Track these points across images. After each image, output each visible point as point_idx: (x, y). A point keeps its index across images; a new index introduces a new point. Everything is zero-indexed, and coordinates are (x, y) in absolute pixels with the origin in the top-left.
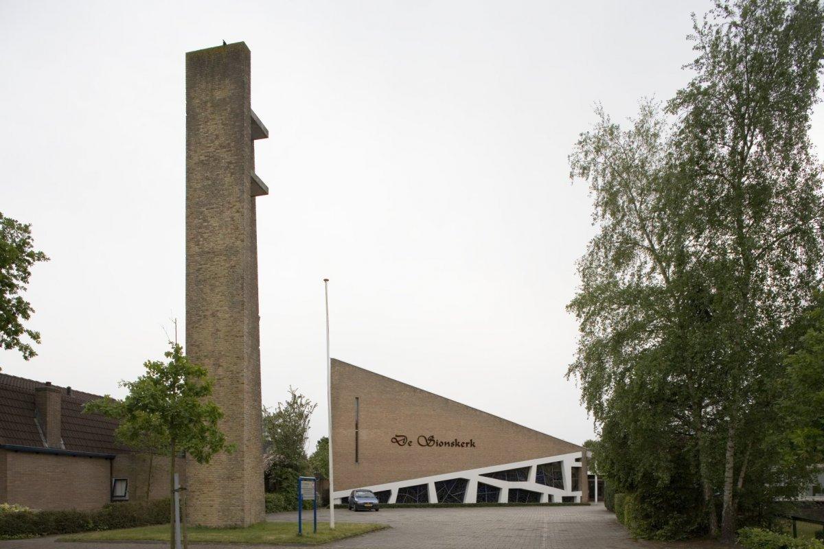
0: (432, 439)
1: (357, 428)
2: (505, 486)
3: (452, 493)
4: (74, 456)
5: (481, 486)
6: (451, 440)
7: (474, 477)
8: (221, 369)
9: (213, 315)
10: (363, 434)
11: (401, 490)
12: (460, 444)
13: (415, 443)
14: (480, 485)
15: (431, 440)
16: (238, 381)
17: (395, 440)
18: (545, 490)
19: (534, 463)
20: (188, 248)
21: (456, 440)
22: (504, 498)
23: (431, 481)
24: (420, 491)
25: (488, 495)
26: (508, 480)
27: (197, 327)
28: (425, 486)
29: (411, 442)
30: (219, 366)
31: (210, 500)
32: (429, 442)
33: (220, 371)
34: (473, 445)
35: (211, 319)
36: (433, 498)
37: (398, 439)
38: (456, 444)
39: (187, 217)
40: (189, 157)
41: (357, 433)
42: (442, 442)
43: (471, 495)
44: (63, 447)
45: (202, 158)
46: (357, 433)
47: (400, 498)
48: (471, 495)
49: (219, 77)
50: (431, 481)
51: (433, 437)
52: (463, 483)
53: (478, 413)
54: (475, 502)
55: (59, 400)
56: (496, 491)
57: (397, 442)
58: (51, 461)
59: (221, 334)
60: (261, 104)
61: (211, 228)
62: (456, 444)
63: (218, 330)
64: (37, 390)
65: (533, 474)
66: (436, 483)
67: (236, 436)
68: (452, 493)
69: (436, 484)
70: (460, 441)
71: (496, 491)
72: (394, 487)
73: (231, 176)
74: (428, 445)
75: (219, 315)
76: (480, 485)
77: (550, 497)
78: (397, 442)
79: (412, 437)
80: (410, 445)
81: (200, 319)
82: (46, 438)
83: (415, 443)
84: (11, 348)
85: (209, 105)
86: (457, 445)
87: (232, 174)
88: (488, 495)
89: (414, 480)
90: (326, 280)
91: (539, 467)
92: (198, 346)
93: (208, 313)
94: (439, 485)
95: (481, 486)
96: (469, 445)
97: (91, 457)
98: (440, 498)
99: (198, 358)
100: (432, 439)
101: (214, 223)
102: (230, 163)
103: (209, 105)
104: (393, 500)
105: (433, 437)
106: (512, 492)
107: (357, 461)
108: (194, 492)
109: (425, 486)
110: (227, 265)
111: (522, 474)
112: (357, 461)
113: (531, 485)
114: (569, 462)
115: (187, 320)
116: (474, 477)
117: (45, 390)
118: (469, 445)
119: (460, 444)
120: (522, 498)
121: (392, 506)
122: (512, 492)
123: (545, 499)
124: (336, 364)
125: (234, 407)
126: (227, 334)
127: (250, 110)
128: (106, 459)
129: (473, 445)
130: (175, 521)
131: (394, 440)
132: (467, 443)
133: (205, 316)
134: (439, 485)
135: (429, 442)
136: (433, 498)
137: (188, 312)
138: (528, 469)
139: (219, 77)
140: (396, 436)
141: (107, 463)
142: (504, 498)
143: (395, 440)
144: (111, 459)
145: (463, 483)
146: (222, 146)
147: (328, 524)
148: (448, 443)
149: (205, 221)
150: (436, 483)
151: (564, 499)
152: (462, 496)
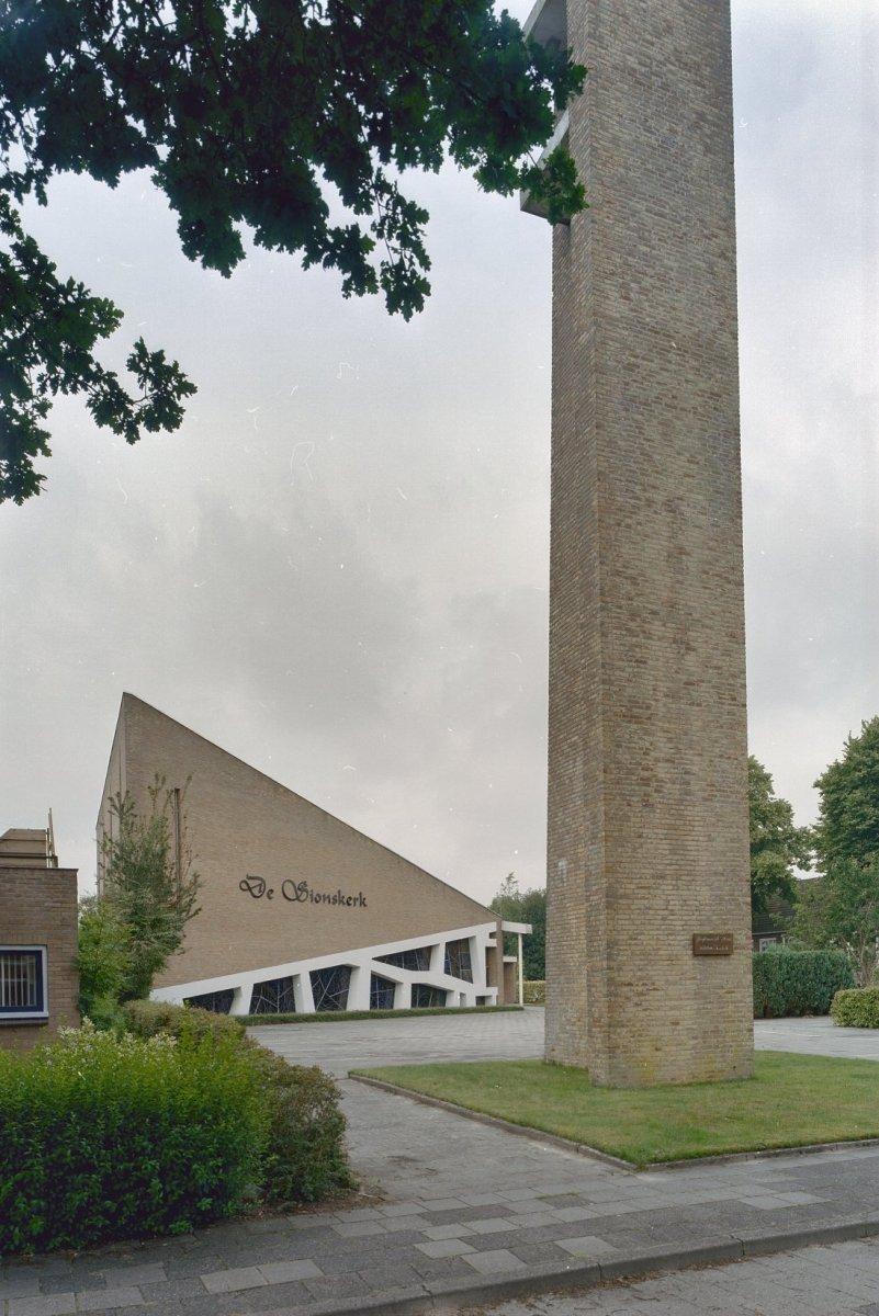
0: (301, 888)
2: (406, 978)
6: (333, 892)
7: (365, 961)
9: (671, 506)
11: (258, 988)
13: (277, 894)
16: (734, 699)
19: (440, 939)
21: (339, 892)
24: (282, 990)
27: (628, 526)
29: (272, 891)
30: (689, 648)
34: (363, 903)
35: (665, 516)
37: (252, 883)
38: (338, 899)
42: (349, 905)
57: (250, 889)
62: (338, 899)
63: (682, 551)
67: (732, 841)
69: (314, 975)
74: (298, 898)
78: (250, 889)
83: (277, 894)
84: (101, 420)
89: (314, 960)
91: (448, 945)
92: (633, 581)
99: (633, 616)
100: (302, 888)
108: (630, 984)
110: (702, 386)
113: (436, 976)
114: (481, 936)
116: (365, 961)
118: (358, 903)
120: (428, 998)
121: (404, 1014)
125: (725, 765)
126: (707, 567)
129: (363, 903)
130: (403, 1067)
132: (355, 899)
133: (650, 503)
135: (299, 893)
138: (430, 949)
148: (329, 897)
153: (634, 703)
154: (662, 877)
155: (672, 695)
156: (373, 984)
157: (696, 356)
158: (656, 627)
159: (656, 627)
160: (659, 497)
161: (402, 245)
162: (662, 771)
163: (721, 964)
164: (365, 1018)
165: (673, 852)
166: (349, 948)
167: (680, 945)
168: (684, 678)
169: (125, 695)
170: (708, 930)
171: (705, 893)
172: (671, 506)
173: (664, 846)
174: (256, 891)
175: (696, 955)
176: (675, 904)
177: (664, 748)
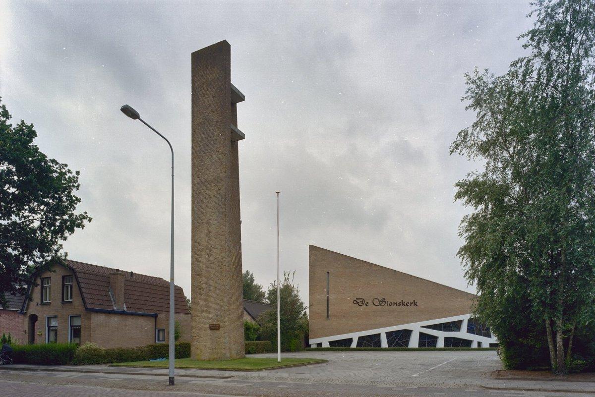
0: (383, 300)
1: (328, 294)
2: (441, 335)
3: (399, 340)
4: (132, 314)
5: (422, 335)
6: (399, 301)
7: (416, 328)
8: (212, 257)
9: (208, 222)
10: (332, 297)
11: (360, 338)
12: (405, 304)
13: (370, 304)
14: (421, 334)
15: (383, 302)
17: (356, 302)
18: (475, 338)
20: (193, 179)
22: (440, 344)
23: (383, 331)
25: (427, 342)
26: (445, 331)
28: (379, 335)
31: (205, 342)
32: (381, 303)
33: (212, 258)
34: (415, 304)
35: (206, 225)
36: (384, 344)
37: (358, 301)
38: (402, 304)
39: (193, 160)
40: (193, 121)
41: (328, 298)
42: (407, 306)
43: (414, 342)
44: (125, 309)
45: (201, 120)
46: (328, 298)
47: (359, 344)
48: (414, 342)
49: (211, 63)
50: (383, 331)
51: (384, 299)
52: (407, 333)
53: (195, 284)
54: (443, 347)
55: (123, 280)
56: (435, 338)
58: (117, 320)
59: (212, 234)
60: (237, 79)
61: (206, 166)
62: (402, 304)
63: (210, 232)
64: (112, 274)
65: (465, 326)
66: (387, 333)
68: (399, 340)
70: (406, 301)
71: (435, 338)
72: (355, 336)
73: (218, 130)
74: (380, 305)
75: (211, 221)
76: (421, 334)
77: (479, 344)
79: (368, 300)
80: (367, 305)
81: (200, 225)
82: (115, 303)
83: (370, 304)
85: (205, 85)
86: (403, 304)
87: (219, 129)
88: (427, 342)
90: (278, 193)
92: (199, 243)
93: (204, 221)
94: (388, 334)
95: (422, 335)
96: (413, 305)
97: (142, 316)
98: (390, 344)
100: (383, 300)
101: (208, 162)
102: (217, 122)
103: (205, 85)
104: (354, 345)
105: (384, 299)
106: (448, 341)
107: (328, 316)
109: (379, 335)
111: (456, 326)
112: (328, 316)
113: (463, 334)
115: (192, 226)
116: (416, 328)
117: (115, 274)
118: (413, 305)
119: (405, 304)
122: (448, 341)
123: (475, 345)
124: (312, 248)
127: (230, 84)
128: (152, 316)
129: (415, 304)
131: (355, 302)
134: (388, 334)
135: (381, 303)
136: (384, 344)
137: (193, 221)
138: (461, 322)
139: (211, 63)
140: (357, 299)
141: (153, 319)
142: (440, 344)
143: (356, 302)
144: (155, 317)
145: (407, 333)
146: (212, 112)
147: (277, 359)
148: (396, 303)
149: (203, 161)
150: (387, 333)
151: (491, 345)
152: (407, 343)
153: (198, 271)
154: (203, 311)
155: (207, 267)
156: (420, 336)
157: (215, 183)
158: (204, 252)
159: (204, 252)
160: (204, 221)
161: (48, 253)
162: (204, 286)
163: (217, 332)
164: (328, 351)
165: (206, 305)
166: (407, 323)
167: (207, 327)
168: (210, 262)
169: (310, 246)
170: (214, 323)
171: (213, 314)
172: (208, 222)
173: (204, 304)
174: (360, 304)
175: (211, 329)
176: (206, 317)
177: (205, 280)
